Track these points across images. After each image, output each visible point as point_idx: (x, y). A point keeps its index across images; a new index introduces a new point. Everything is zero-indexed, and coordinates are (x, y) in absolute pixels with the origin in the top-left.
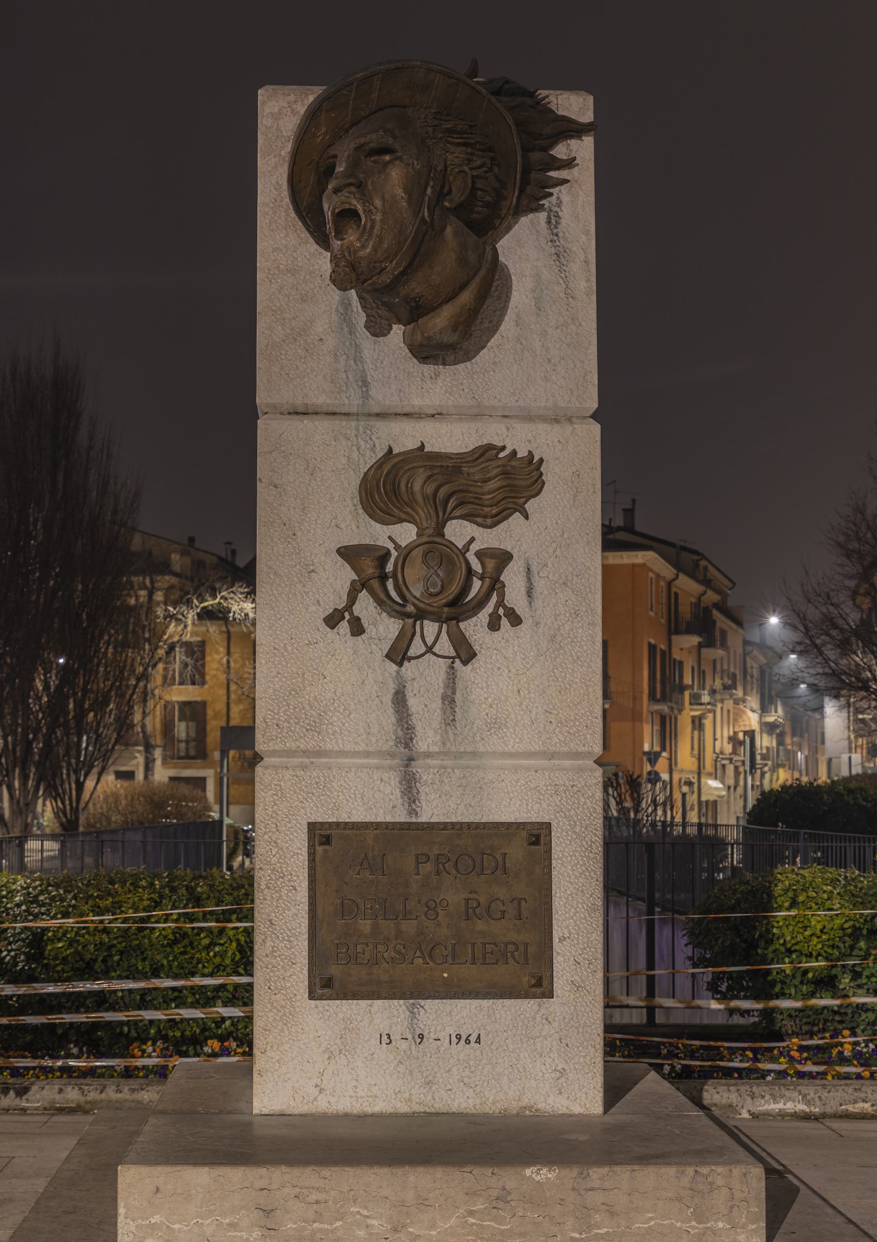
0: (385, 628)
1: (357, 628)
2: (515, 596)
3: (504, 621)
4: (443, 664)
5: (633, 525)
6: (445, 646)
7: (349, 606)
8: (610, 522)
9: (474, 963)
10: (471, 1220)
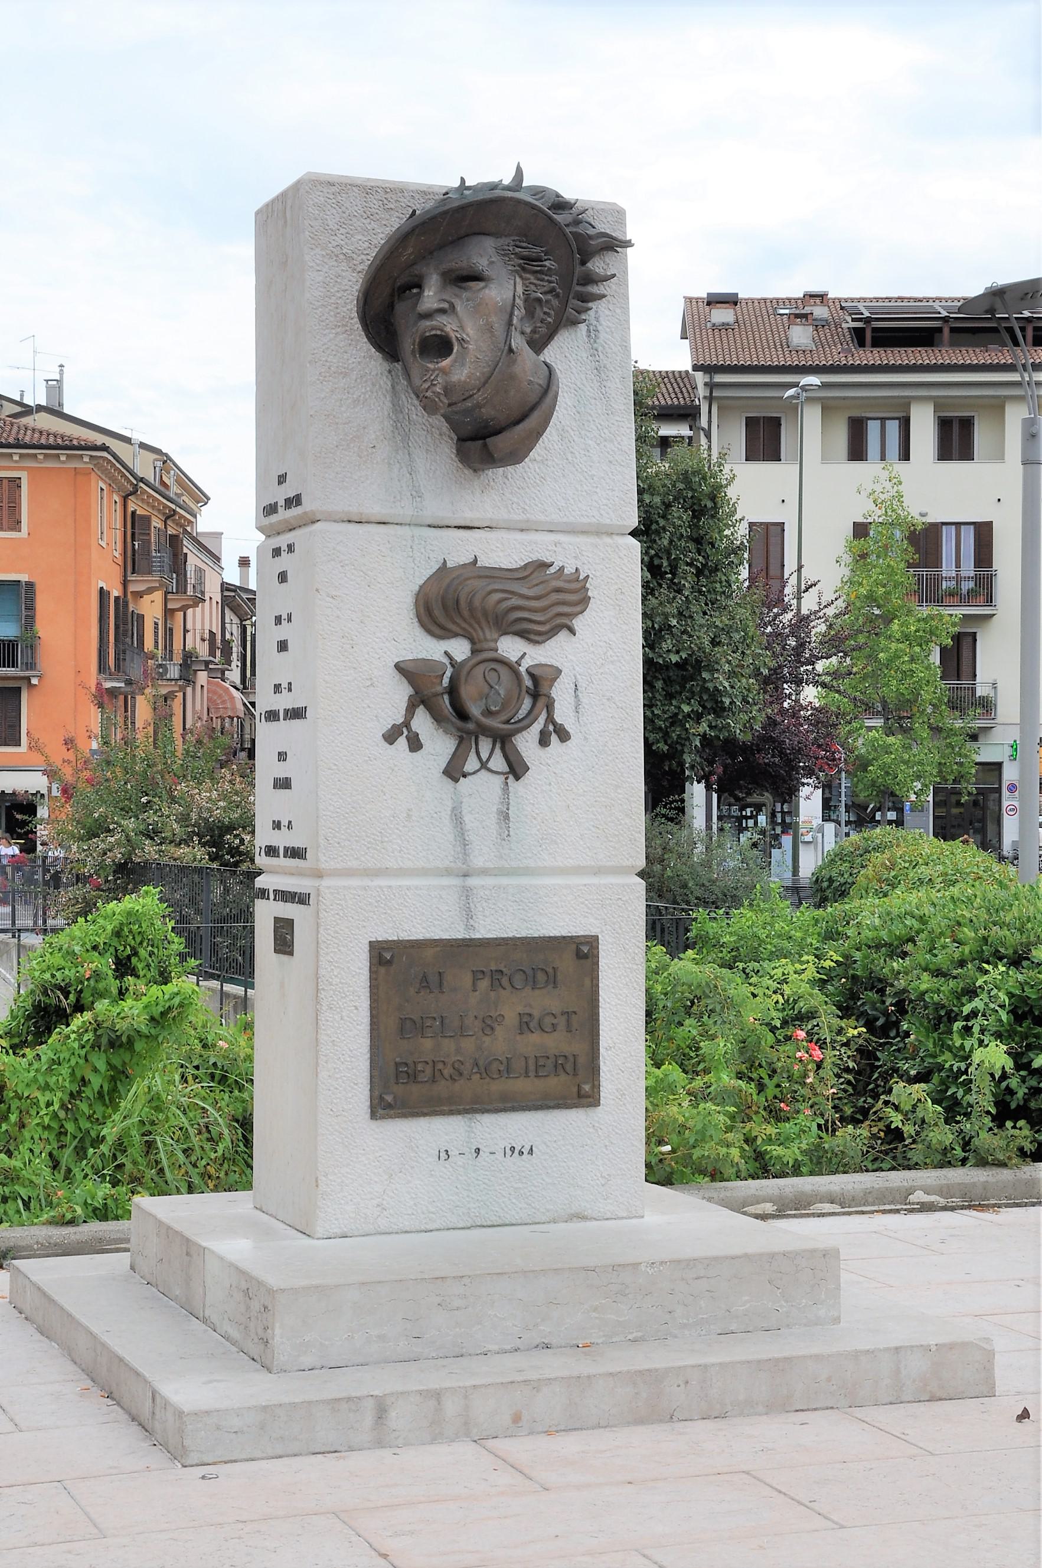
0: (439, 745)
1: (415, 744)
2: (563, 714)
3: (554, 738)
4: (499, 780)
5: (61, 405)
6: (498, 762)
7: (407, 724)
8: (22, 396)
9: (527, 1076)
10: (594, 1314)
